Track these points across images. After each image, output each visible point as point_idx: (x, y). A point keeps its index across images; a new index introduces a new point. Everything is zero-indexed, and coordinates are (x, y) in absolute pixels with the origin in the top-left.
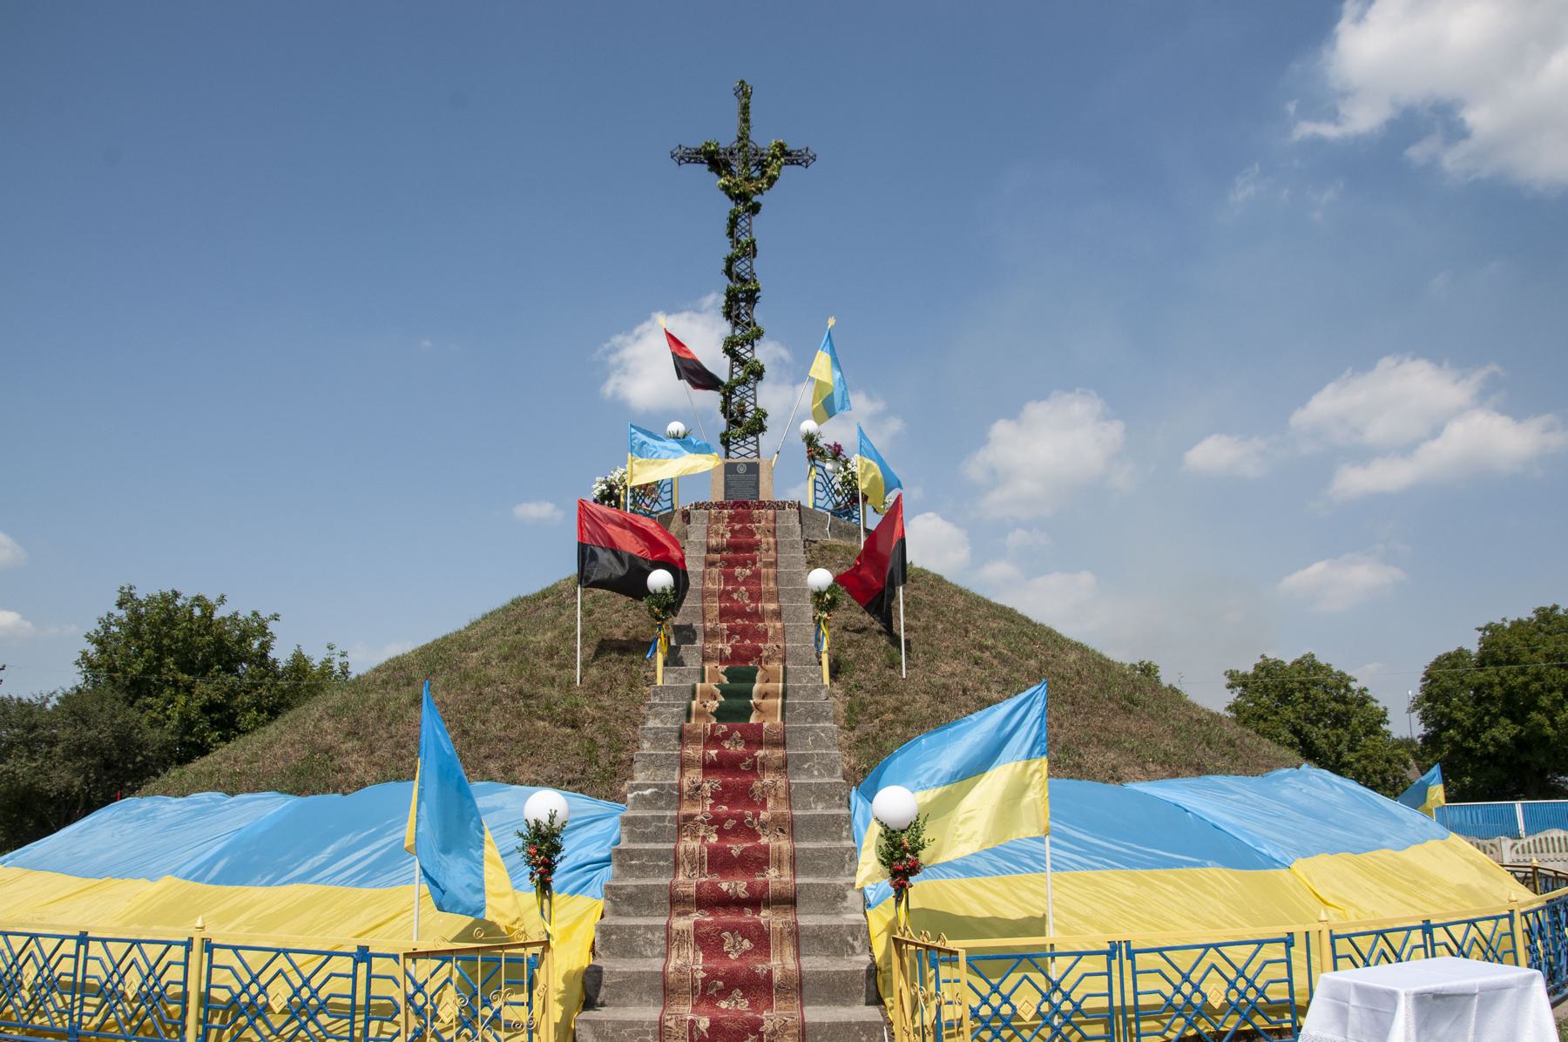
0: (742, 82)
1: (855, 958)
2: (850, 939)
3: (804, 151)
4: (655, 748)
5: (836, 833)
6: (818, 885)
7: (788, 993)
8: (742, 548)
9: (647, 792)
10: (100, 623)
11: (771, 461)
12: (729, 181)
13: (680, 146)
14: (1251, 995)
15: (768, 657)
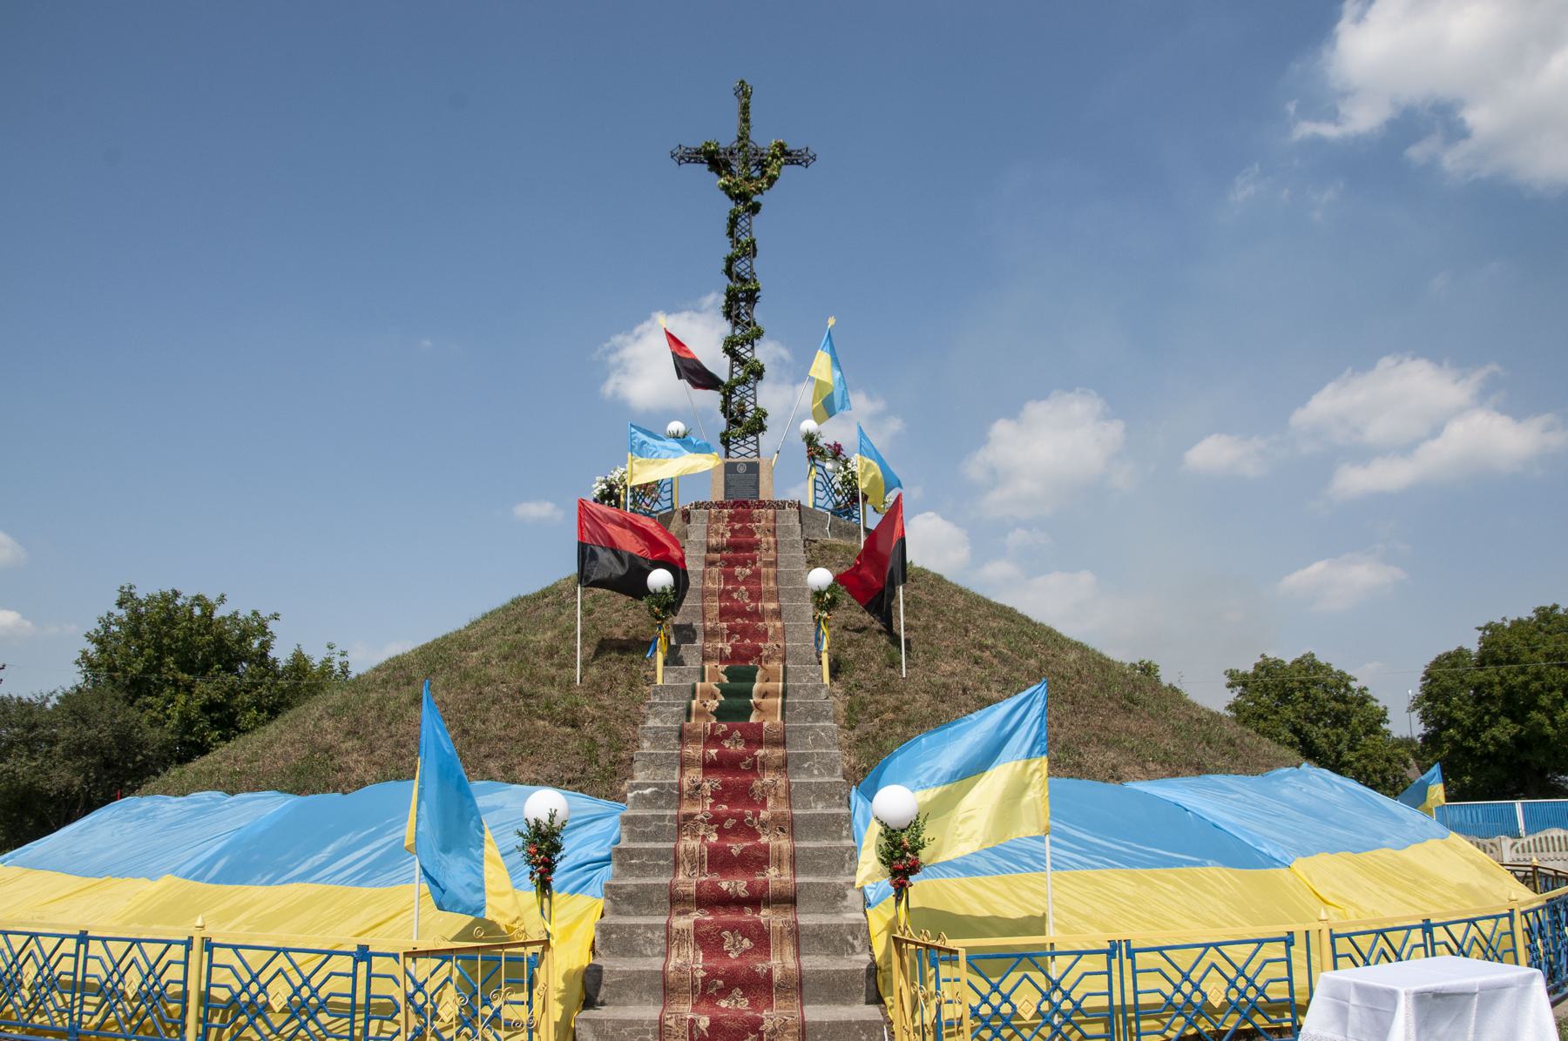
0: (742, 82)
1: (855, 957)
2: (850, 938)
3: (804, 151)
4: (655, 748)
6: (818, 884)
7: (788, 992)
8: (742, 548)
9: (647, 791)
10: (100, 622)
11: (771, 461)
12: (729, 181)
13: (680, 146)
14: (1251, 994)
15: (768, 656)
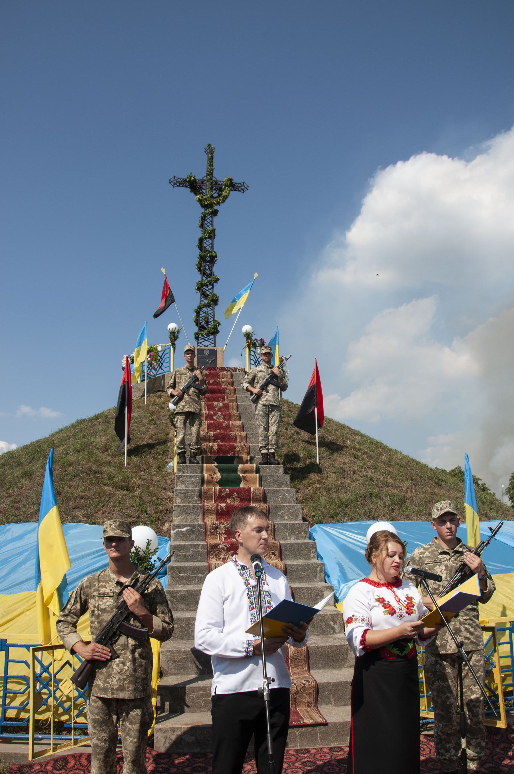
0: (209, 145)
1: (336, 636)
2: (332, 623)
3: (242, 184)
4: (184, 502)
5: (307, 554)
6: (306, 588)
7: (299, 662)
9: (184, 529)
11: (223, 349)
12: (202, 197)
13: (174, 177)
